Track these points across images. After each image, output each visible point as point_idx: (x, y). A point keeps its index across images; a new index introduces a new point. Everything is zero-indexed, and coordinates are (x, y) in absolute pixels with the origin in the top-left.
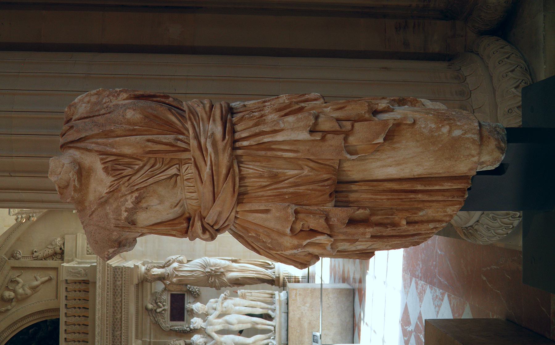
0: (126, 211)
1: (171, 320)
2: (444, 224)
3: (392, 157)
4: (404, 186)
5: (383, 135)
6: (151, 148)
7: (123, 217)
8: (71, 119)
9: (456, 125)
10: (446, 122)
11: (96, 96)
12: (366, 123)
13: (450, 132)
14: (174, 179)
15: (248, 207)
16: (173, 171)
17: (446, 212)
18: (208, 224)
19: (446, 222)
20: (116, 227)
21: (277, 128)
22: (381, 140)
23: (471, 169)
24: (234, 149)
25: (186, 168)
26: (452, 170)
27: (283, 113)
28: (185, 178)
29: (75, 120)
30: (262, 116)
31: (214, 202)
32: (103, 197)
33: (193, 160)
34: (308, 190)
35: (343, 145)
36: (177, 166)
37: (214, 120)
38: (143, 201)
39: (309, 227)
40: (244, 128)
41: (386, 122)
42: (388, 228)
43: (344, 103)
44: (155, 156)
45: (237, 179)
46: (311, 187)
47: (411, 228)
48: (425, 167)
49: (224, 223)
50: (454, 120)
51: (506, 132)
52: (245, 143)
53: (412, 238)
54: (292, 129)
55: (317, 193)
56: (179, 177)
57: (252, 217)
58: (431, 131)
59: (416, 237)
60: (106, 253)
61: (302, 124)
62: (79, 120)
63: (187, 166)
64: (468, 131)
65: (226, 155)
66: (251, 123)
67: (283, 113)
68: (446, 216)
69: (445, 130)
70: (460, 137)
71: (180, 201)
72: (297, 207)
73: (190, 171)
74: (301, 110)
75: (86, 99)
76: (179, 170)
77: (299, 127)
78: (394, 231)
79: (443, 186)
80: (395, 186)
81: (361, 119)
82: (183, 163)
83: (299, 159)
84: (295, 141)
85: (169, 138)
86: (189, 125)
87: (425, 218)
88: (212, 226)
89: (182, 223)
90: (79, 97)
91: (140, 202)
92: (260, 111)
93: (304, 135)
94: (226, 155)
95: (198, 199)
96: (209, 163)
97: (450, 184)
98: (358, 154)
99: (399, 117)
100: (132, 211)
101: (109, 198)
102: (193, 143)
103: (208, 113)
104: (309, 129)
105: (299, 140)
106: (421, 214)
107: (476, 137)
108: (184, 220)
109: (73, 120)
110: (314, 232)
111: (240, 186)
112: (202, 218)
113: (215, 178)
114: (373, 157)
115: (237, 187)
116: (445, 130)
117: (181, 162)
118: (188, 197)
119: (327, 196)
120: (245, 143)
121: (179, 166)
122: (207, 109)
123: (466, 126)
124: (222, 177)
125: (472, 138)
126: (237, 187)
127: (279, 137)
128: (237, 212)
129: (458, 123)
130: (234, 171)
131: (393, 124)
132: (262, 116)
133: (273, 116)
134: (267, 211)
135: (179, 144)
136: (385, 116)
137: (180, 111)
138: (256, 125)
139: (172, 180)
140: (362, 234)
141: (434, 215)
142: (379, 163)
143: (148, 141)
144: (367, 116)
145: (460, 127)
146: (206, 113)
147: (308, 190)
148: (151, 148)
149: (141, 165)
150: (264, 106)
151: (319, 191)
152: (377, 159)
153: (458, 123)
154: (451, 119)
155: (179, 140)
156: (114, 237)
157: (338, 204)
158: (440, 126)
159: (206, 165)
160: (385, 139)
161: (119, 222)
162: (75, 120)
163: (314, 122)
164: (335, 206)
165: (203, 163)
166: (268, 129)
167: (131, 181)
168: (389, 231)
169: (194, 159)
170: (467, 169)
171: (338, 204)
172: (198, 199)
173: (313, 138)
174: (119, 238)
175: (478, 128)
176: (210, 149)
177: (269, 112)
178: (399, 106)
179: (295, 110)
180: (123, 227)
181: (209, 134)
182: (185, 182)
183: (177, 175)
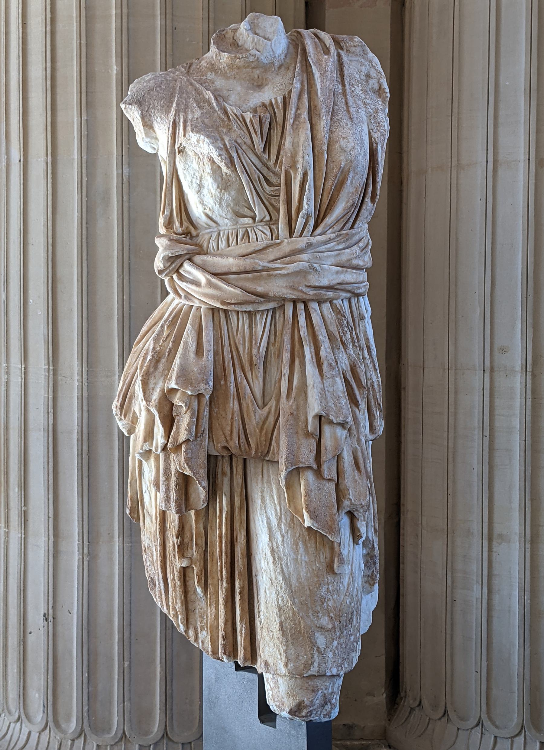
1: (170, 293)
2: (182, 629)
3: (283, 540)
4: (240, 561)
5: (316, 525)
6: (295, 178)
8: (342, 49)
9: (333, 640)
10: (337, 623)
11: (376, 86)
12: (335, 501)
13: (322, 629)
16: (259, 211)
17: (201, 630)
21: (325, 367)
22: (308, 523)
23: (267, 664)
24: (295, 302)
25: (265, 231)
27: (349, 376)
29: (339, 55)
30: (343, 343)
33: (278, 241)
34: (233, 414)
35: (301, 465)
36: (268, 218)
37: (337, 273)
40: (326, 318)
41: (333, 529)
42: (177, 538)
43: (366, 468)
44: (283, 187)
45: (249, 308)
46: (237, 418)
49: (183, 289)
50: (340, 637)
51: (324, 720)
52: (302, 320)
53: (161, 577)
54: (323, 389)
55: (229, 428)
56: (250, 221)
58: (323, 600)
59: (162, 584)
61: (331, 404)
63: (269, 233)
64: (324, 658)
65: (285, 291)
66: (333, 328)
67: (349, 376)
69: (325, 621)
70: (313, 644)
72: (207, 397)
74: (353, 401)
75: (373, 73)
76: (261, 221)
77: (326, 399)
78: (172, 548)
79: (241, 621)
80: (240, 548)
81: (340, 494)
82: (272, 226)
83: (278, 400)
85: (308, 206)
86: (330, 235)
87: (191, 596)
88: (177, 271)
89: (181, 225)
90: (376, 60)
92: (353, 342)
93: (314, 407)
94: (285, 291)
95: (218, 249)
96: (271, 265)
97: (243, 632)
98: (287, 489)
99: (345, 552)
102: (301, 242)
103: (348, 264)
104: (324, 414)
105: (307, 400)
106: (199, 590)
107: (314, 670)
108: (187, 228)
109: (340, 51)
110: (169, 422)
111: (238, 312)
113: (250, 275)
115: (237, 308)
116: (325, 621)
120: (302, 320)
121: (268, 221)
122: (355, 262)
123: (331, 655)
124: (250, 286)
125: (312, 663)
126: (237, 308)
127: (311, 369)
129: (335, 643)
130: (261, 303)
131: (333, 542)
132: (343, 343)
133: (344, 363)
134: (199, 351)
135: (301, 220)
136: (346, 531)
137: (351, 221)
138: (331, 337)
142: (274, 522)
144: (346, 503)
145: (329, 643)
146: (350, 260)
147: (233, 414)
150: (362, 349)
152: (280, 519)
153: (335, 643)
154: (342, 633)
157: (212, 459)
158: (332, 615)
159: (270, 262)
160: (309, 528)
162: (339, 55)
163: (335, 421)
164: (209, 456)
165: (272, 257)
166: (323, 353)
168: (172, 540)
169: (279, 244)
170: (267, 658)
172: (218, 249)
173: (310, 419)
175: (328, 674)
176: (292, 268)
177: (350, 355)
178: (364, 556)
179: (354, 394)
181: (315, 265)
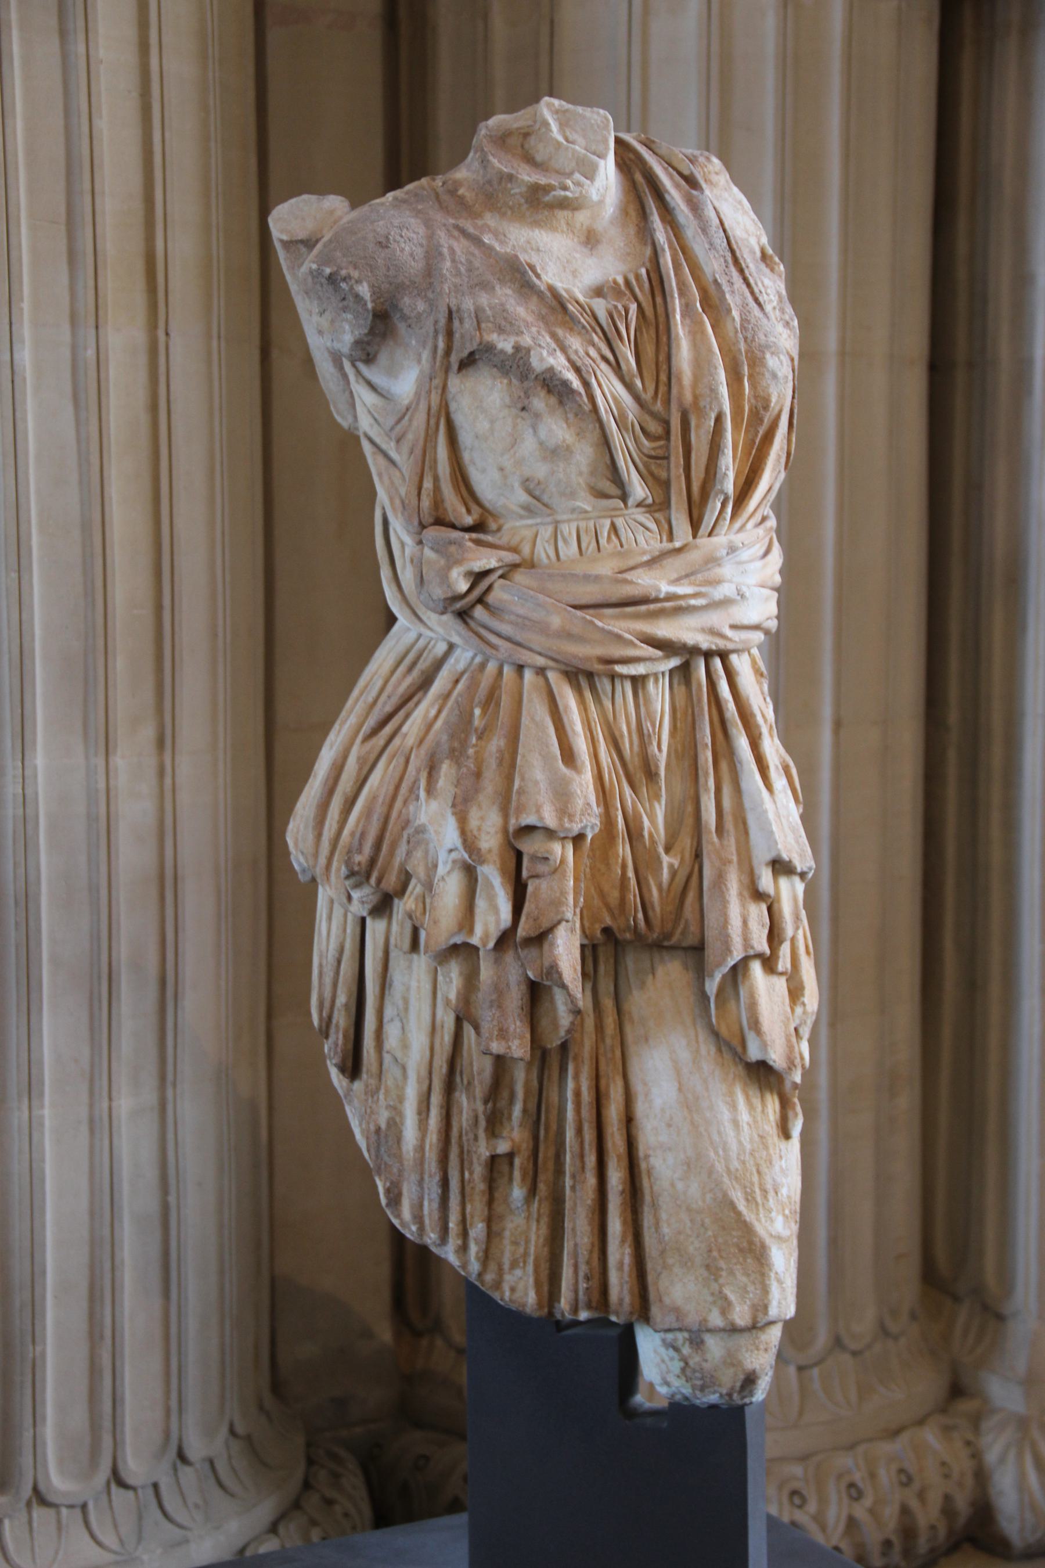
0: (517, 348)
6: (698, 426)
7: (493, 337)
14: (613, 490)
15: (568, 699)
16: (639, 490)
18: (490, 588)
19: (480, 1275)
20: (450, 312)
26: (670, 1261)
28: (620, 522)
31: (575, 607)
32: (538, 276)
38: (553, 400)
39: (537, 876)
47: (478, 1171)
48: (680, 1186)
57: (536, 710)
60: (355, 274)
62: (715, 208)
63: (653, 526)
68: (500, 1269)
71: (546, 505)
73: (641, 540)
80: (614, 1112)
82: (657, 515)
84: (745, 823)
91: (549, 391)
100: (516, 367)
101: (540, 294)
112: (508, 571)
114: (701, 1038)
117: (659, 506)
118: (565, 528)
119: (608, 921)
128: (541, 671)
139: (608, 483)
140: (501, 1030)
141: (507, 1233)
142: (684, 1055)
143: (719, 419)
148: (698, 426)
149: (643, 396)
151: (623, 900)
152: (698, 1051)
155: (724, 505)
156: (407, 300)
161: (469, 324)
167: (603, 366)
171: (588, 953)
174: (404, 318)
180: (450, 334)
182: (607, 523)
183: (624, 497)
